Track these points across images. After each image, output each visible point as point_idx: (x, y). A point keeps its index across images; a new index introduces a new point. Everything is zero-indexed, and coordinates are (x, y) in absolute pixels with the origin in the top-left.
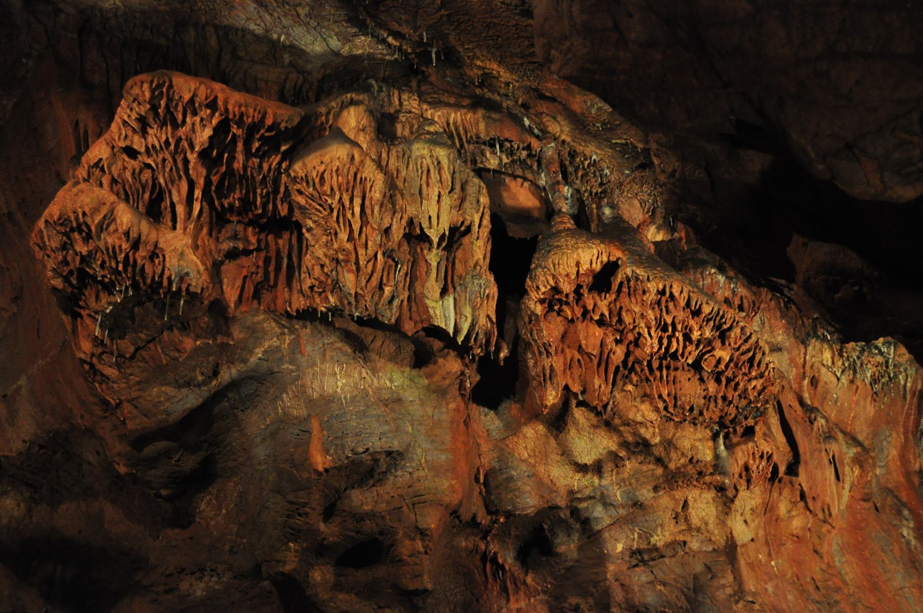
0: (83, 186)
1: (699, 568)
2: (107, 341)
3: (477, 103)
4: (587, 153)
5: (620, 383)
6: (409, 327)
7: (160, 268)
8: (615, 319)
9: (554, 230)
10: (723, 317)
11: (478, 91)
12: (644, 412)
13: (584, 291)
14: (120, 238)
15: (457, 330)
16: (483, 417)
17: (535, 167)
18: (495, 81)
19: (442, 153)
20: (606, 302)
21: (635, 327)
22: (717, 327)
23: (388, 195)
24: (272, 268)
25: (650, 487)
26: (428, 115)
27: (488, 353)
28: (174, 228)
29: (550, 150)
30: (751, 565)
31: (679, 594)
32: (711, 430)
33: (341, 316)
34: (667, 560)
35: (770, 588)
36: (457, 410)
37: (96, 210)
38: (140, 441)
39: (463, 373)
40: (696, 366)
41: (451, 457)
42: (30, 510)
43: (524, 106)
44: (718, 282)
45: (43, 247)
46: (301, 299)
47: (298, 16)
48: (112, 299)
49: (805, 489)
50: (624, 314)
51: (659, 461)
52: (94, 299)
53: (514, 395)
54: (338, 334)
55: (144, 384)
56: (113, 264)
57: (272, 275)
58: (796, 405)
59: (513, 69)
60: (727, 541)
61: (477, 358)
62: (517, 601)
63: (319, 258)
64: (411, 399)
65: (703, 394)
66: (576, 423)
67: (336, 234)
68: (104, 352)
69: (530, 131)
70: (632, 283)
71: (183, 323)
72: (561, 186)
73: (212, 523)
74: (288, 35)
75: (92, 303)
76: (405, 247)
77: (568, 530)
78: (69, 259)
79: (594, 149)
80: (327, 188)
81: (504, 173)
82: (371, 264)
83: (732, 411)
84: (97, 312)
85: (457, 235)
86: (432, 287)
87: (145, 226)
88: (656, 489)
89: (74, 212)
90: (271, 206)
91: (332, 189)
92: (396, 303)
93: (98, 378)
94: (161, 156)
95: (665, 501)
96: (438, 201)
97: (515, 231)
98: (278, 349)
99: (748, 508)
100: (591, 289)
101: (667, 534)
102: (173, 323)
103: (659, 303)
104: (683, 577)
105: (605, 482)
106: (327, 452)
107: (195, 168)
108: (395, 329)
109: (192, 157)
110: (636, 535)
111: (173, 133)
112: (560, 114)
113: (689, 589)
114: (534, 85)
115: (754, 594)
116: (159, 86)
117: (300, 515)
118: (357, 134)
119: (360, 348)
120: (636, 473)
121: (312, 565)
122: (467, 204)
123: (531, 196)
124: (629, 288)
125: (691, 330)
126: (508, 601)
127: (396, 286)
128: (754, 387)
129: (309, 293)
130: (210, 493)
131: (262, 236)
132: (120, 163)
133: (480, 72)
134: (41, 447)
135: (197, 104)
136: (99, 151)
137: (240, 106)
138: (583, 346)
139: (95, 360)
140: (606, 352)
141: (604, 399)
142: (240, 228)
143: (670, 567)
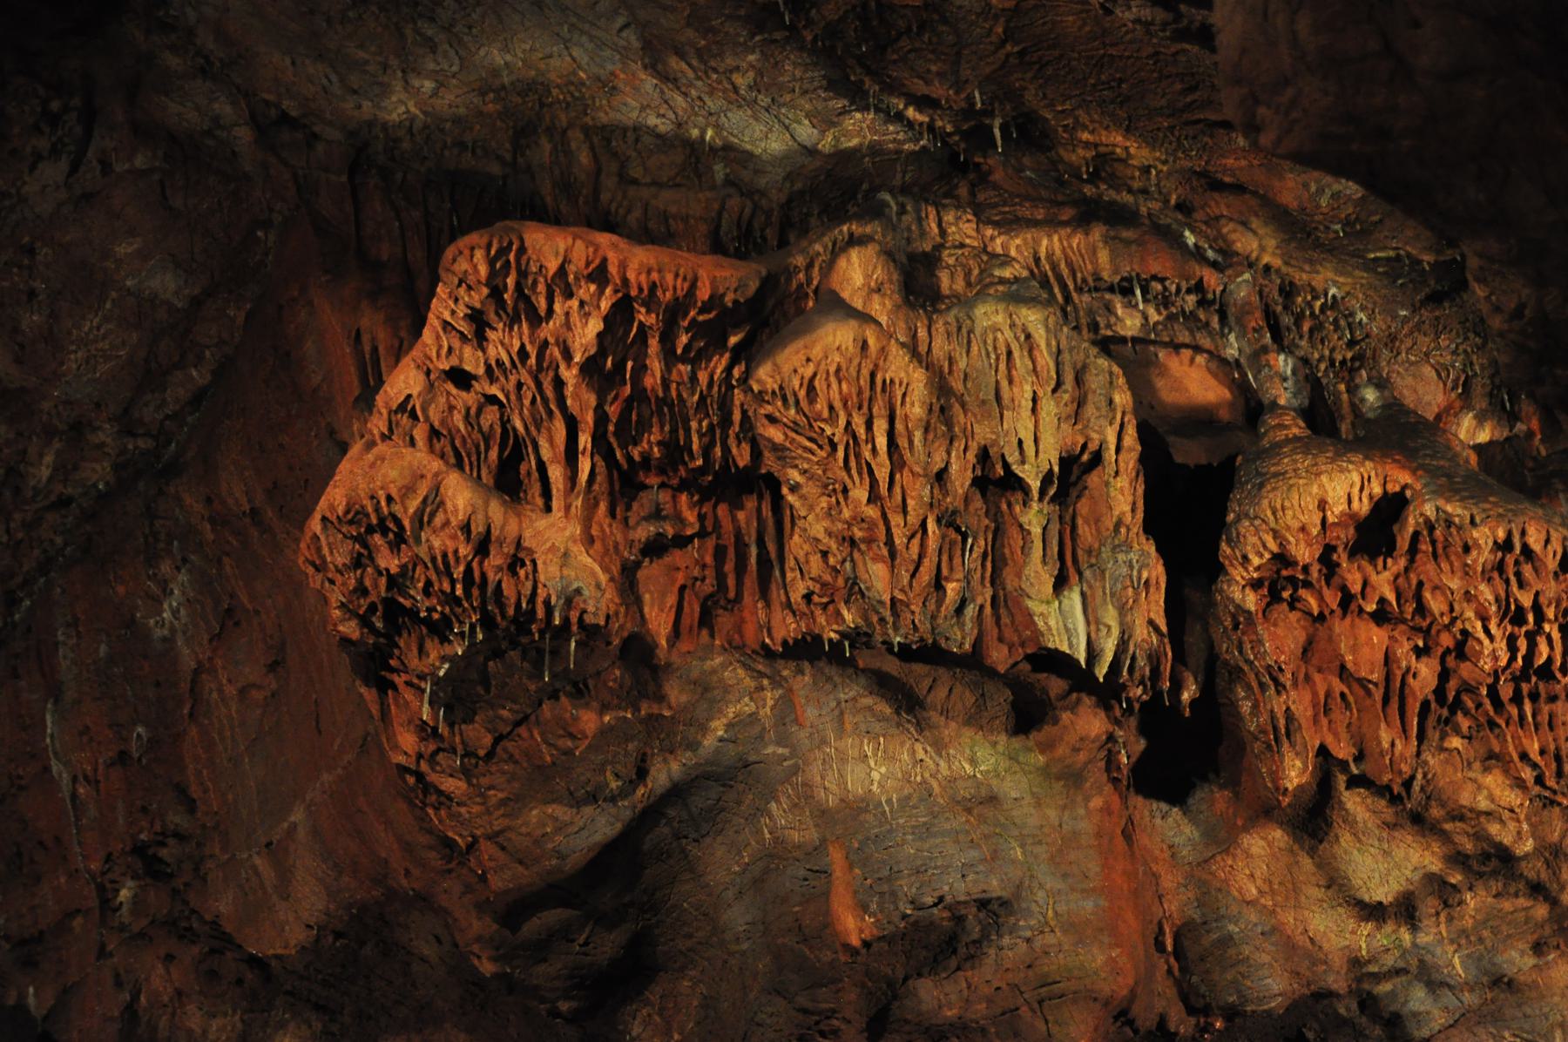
0: (382, 447)
3: (1088, 214)
5: (1433, 735)
6: (999, 657)
7: (529, 584)
8: (1410, 608)
9: (1265, 443)
11: (1088, 190)
12: (1492, 791)
13: (1341, 557)
14: (454, 537)
15: (1093, 654)
16: (1158, 821)
17: (1215, 322)
18: (1119, 167)
19: (1032, 318)
20: (1387, 575)
21: (1453, 621)
23: (936, 408)
24: (729, 567)
26: (997, 246)
27: (1157, 694)
28: (548, 509)
29: (1242, 287)
33: (868, 646)
36: (1107, 810)
37: (409, 490)
38: (514, 911)
39: (1111, 738)
41: (1103, 903)
47: (736, 89)
48: (447, 650)
50: (1427, 595)
51: (1537, 889)
54: (862, 680)
55: (515, 803)
56: (446, 586)
57: (731, 581)
61: (1137, 706)
63: (818, 540)
67: (845, 491)
68: (439, 750)
70: (1438, 533)
71: (575, 685)
72: (1271, 356)
74: (718, 127)
75: (413, 662)
76: (978, 503)
78: (367, 583)
79: (1330, 275)
81: (1154, 342)
82: (916, 541)
84: (422, 677)
85: (1076, 471)
86: (1037, 574)
88: (1538, 948)
89: (372, 498)
90: (718, 451)
91: (831, 408)
92: (970, 611)
94: (513, 379)
100: (1354, 552)
102: (558, 685)
103: (1500, 567)
105: (1424, 939)
106: (864, 908)
107: (576, 395)
108: (973, 662)
109: (569, 375)
111: (532, 335)
119: (907, 704)
120: (1488, 919)
122: (1090, 410)
124: (1433, 542)
129: (803, 607)
133: (1090, 154)
136: (404, 382)
137: (649, 272)
138: (1349, 666)
139: (424, 767)
140: (1399, 674)
141: (1405, 768)
142: (664, 497)
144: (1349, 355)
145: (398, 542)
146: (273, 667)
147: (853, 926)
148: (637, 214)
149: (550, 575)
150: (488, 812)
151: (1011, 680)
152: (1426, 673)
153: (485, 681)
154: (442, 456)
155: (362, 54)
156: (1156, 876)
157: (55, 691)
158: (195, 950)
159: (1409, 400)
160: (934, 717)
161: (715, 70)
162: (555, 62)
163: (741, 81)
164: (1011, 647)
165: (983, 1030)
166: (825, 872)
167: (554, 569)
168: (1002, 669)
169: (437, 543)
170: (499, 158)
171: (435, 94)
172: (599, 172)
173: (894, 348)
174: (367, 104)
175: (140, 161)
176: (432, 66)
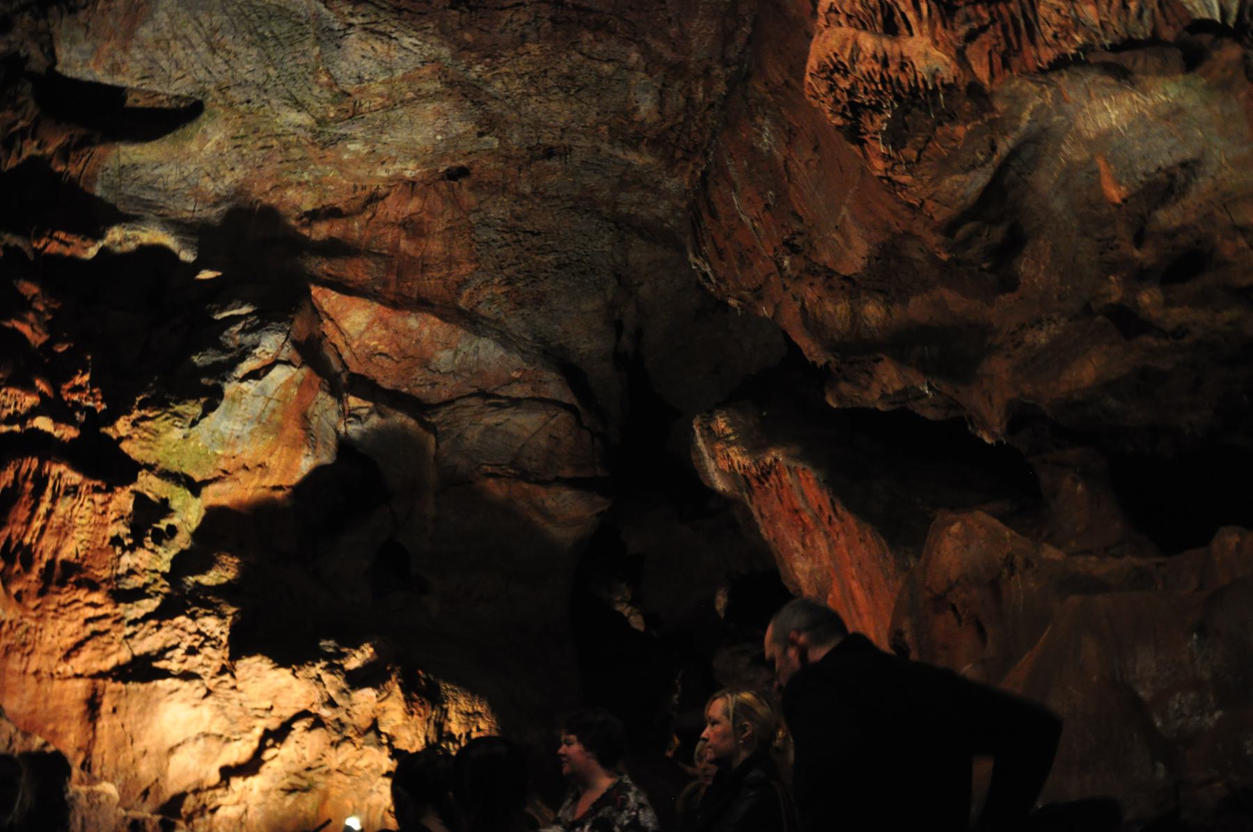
0: (826, 32)
6: (1168, 34)
24: (1011, 34)
28: (911, 34)
37: (843, 47)
38: (950, 228)
48: (884, 117)
55: (936, 180)
57: (1014, 41)
75: (870, 127)
84: (876, 133)
92: (1146, 14)
106: (1119, 183)
108: (1154, 41)
119: (1122, 75)
139: (890, 174)
142: (969, 10)
145: (846, 73)
146: (816, 149)
147: (1115, 193)
149: (921, 66)
151: (1179, 44)
154: (856, 27)
157: (733, 186)
158: (821, 279)
160: (1139, 77)
166: (1097, 172)
167: (922, 63)
168: (1171, 39)
169: (863, 68)
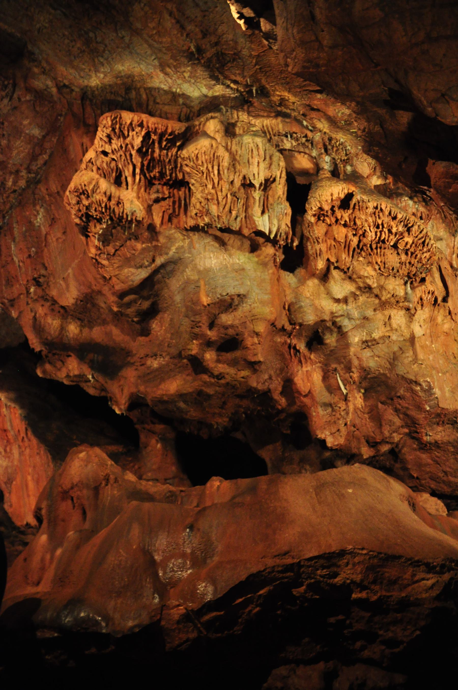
0: (84, 172)
1: (396, 349)
2: (101, 247)
3: (278, 114)
4: (338, 138)
5: (356, 257)
6: (246, 232)
7: (122, 209)
8: (352, 223)
9: (319, 178)
10: (408, 220)
11: (279, 109)
12: (368, 271)
13: (336, 209)
14: (102, 196)
15: (270, 232)
16: (287, 277)
17: (310, 146)
18: (287, 102)
19: (259, 140)
20: (347, 214)
21: (363, 227)
22: (406, 226)
23: (232, 164)
24: (177, 206)
25: (372, 310)
26: (253, 122)
27: (287, 244)
28: (127, 189)
29: (317, 137)
30: (422, 347)
31: (386, 361)
32: (404, 280)
33: (212, 227)
34: (380, 345)
35: (431, 358)
36: (273, 273)
37: (90, 183)
38: (122, 295)
39: (275, 255)
40: (395, 246)
41: (270, 297)
42: (81, 330)
43: (304, 115)
44: (409, 205)
45: (69, 204)
46: (192, 220)
47: (185, 77)
48: (101, 226)
49: (451, 309)
50: (357, 220)
51: (377, 296)
52: (93, 227)
53: (302, 265)
54: (211, 237)
55: (120, 267)
56: (100, 209)
57: (177, 210)
58: (448, 267)
59: (296, 95)
60: (410, 335)
61: (282, 246)
62: (306, 367)
63: (198, 199)
64: (249, 268)
65: (399, 261)
66: (333, 278)
67: (206, 185)
68: (101, 253)
69: (307, 128)
70: (360, 204)
71: (135, 236)
72: (323, 156)
73: (159, 334)
74: (180, 88)
75: (93, 230)
76: (242, 190)
77: (331, 331)
78: (81, 208)
79: (341, 136)
80: (200, 162)
81: (294, 151)
82: (225, 200)
83: (414, 269)
84: (95, 234)
85: (269, 183)
86: (257, 210)
87: (113, 189)
88: (375, 310)
89: (81, 185)
90: (174, 175)
91: (202, 162)
92: (239, 219)
93: (100, 266)
94: (119, 154)
95: (380, 316)
96: (258, 166)
97: (301, 180)
98: (182, 247)
99: (422, 320)
100: (340, 208)
101: (380, 332)
102: (131, 236)
103: (374, 213)
104: (388, 353)
105: (349, 308)
106: (208, 296)
107: (135, 158)
108: (239, 233)
109: (134, 153)
110: (365, 334)
111: (124, 141)
112: (322, 117)
113: (391, 359)
114: (308, 103)
115: (423, 360)
116: (115, 118)
117: (197, 327)
118: (215, 134)
119: (223, 244)
120: (365, 303)
121: (205, 351)
122: (273, 166)
123: (309, 162)
124: (359, 206)
125: (391, 227)
126: (302, 367)
127: (238, 210)
128: (425, 257)
129: (195, 217)
130: (156, 320)
131: (171, 190)
132: (100, 160)
133: (279, 98)
134: (81, 301)
135: (133, 126)
136: (91, 154)
137: (155, 124)
138: (336, 238)
139: (97, 257)
140: (348, 240)
141: (347, 264)
142: (160, 187)
143: (382, 349)
144: (346, 158)
148: (159, 112)
150: (114, 270)
152: (355, 240)
153: (112, 235)
155: (84, 67)
156: (285, 291)
159: (360, 171)
161: (179, 72)
162: (136, 69)
163: (187, 75)
164: (249, 229)
165: (237, 327)
168: (246, 235)
170: (121, 96)
171: (104, 78)
172: (148, 100)
173: (220, 147)
174: (86, 81)
175: (28, 98)
176: (102, 70)
